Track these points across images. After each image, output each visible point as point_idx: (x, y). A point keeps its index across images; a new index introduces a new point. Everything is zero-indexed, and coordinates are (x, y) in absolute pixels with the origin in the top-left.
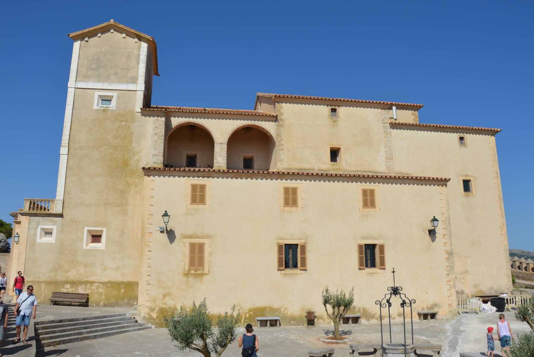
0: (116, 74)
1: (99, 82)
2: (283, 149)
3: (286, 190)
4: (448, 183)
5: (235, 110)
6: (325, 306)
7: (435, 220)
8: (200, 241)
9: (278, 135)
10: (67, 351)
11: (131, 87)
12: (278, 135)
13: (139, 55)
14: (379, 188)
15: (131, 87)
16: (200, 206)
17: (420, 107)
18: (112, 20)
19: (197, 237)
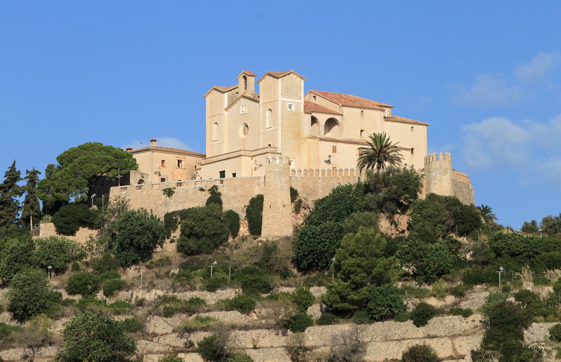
0: (294, 95)
1: (289, 98)
2: (344, 130)
3: (333, 146)
4: (21, 173)
5: (365, 99)
6: (207, 159)
7: (330, 156)
8: (335, 166)
9: (342, 123)
10: (434, 319)
11: (299, 101)
12: (342, 123)
13: (301, 87)
14: (339, 146)
15: (299, 101)
16: (335, 154)
17: (392, 107)
18: (292, 70)
19: (334, 165)
